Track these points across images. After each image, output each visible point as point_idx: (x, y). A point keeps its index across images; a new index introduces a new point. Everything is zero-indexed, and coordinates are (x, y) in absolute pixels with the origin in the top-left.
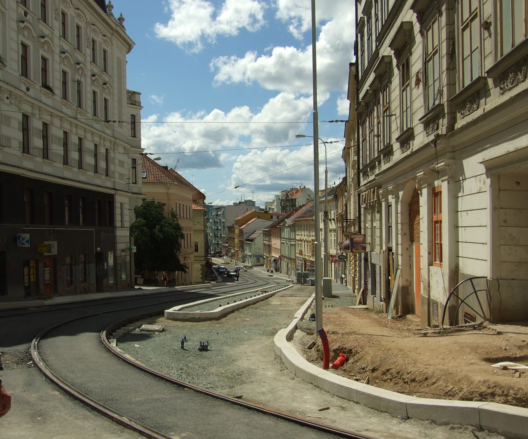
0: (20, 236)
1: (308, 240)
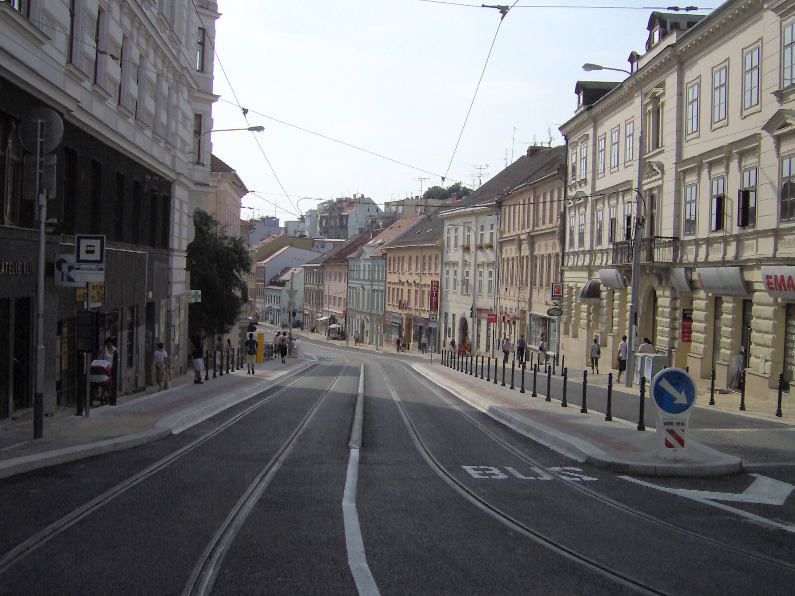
0: (62, 261)
1: (418, 282)
